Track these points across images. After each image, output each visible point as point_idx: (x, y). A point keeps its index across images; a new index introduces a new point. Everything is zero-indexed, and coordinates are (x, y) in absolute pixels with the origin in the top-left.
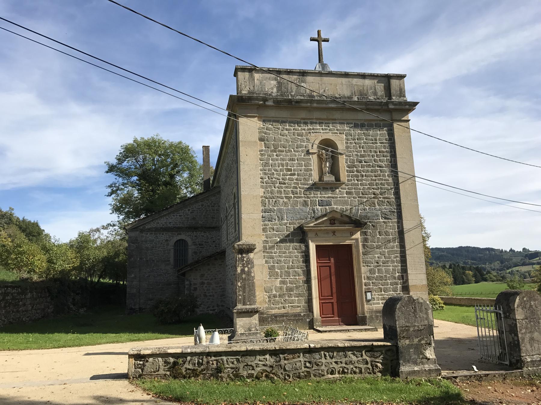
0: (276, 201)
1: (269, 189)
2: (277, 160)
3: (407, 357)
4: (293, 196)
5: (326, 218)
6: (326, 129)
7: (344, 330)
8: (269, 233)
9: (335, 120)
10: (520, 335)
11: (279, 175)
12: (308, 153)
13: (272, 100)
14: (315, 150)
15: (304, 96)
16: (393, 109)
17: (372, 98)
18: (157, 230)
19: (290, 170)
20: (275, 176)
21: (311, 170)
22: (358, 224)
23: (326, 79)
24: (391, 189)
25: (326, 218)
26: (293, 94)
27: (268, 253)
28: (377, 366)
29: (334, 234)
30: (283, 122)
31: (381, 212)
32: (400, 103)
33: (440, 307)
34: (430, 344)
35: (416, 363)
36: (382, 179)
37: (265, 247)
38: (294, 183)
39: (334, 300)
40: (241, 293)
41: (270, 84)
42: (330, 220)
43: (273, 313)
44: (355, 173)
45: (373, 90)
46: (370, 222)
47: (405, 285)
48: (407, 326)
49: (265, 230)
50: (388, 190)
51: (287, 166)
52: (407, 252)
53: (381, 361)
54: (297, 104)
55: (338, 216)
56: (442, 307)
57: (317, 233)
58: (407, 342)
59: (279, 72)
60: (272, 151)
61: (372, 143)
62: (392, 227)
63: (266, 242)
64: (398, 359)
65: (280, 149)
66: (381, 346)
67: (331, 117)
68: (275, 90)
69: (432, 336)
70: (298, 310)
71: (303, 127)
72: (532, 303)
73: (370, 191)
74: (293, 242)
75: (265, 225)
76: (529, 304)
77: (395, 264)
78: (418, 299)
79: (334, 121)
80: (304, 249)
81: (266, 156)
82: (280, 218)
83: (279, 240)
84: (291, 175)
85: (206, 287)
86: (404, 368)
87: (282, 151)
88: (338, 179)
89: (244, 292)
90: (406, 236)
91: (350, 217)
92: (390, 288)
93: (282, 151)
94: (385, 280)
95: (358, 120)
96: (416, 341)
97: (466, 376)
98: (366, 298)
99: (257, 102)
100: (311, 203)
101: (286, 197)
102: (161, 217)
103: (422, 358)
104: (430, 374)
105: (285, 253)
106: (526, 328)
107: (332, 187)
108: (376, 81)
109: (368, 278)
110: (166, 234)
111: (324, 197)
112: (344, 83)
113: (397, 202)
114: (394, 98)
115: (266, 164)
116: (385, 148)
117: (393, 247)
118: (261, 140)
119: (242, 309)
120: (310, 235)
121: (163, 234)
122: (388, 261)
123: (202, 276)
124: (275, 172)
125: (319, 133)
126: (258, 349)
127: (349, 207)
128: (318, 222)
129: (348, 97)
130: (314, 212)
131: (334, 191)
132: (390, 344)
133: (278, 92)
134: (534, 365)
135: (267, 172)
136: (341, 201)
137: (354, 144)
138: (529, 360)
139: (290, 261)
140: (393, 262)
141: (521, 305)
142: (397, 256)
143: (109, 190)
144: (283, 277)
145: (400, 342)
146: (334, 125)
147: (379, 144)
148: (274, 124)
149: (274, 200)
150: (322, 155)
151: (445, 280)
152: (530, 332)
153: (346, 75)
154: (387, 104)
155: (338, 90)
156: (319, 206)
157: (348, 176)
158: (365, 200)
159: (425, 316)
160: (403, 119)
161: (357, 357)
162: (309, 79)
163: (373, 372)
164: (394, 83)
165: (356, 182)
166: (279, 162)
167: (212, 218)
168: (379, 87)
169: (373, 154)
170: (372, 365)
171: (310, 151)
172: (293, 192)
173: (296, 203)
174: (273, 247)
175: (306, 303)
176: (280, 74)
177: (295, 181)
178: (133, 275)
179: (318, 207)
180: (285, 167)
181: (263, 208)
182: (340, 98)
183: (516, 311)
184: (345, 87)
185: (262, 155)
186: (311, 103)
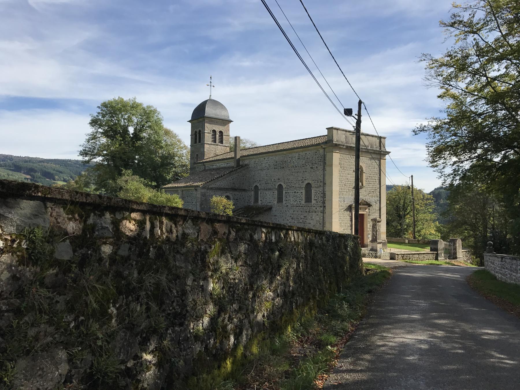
164: (382, 140)
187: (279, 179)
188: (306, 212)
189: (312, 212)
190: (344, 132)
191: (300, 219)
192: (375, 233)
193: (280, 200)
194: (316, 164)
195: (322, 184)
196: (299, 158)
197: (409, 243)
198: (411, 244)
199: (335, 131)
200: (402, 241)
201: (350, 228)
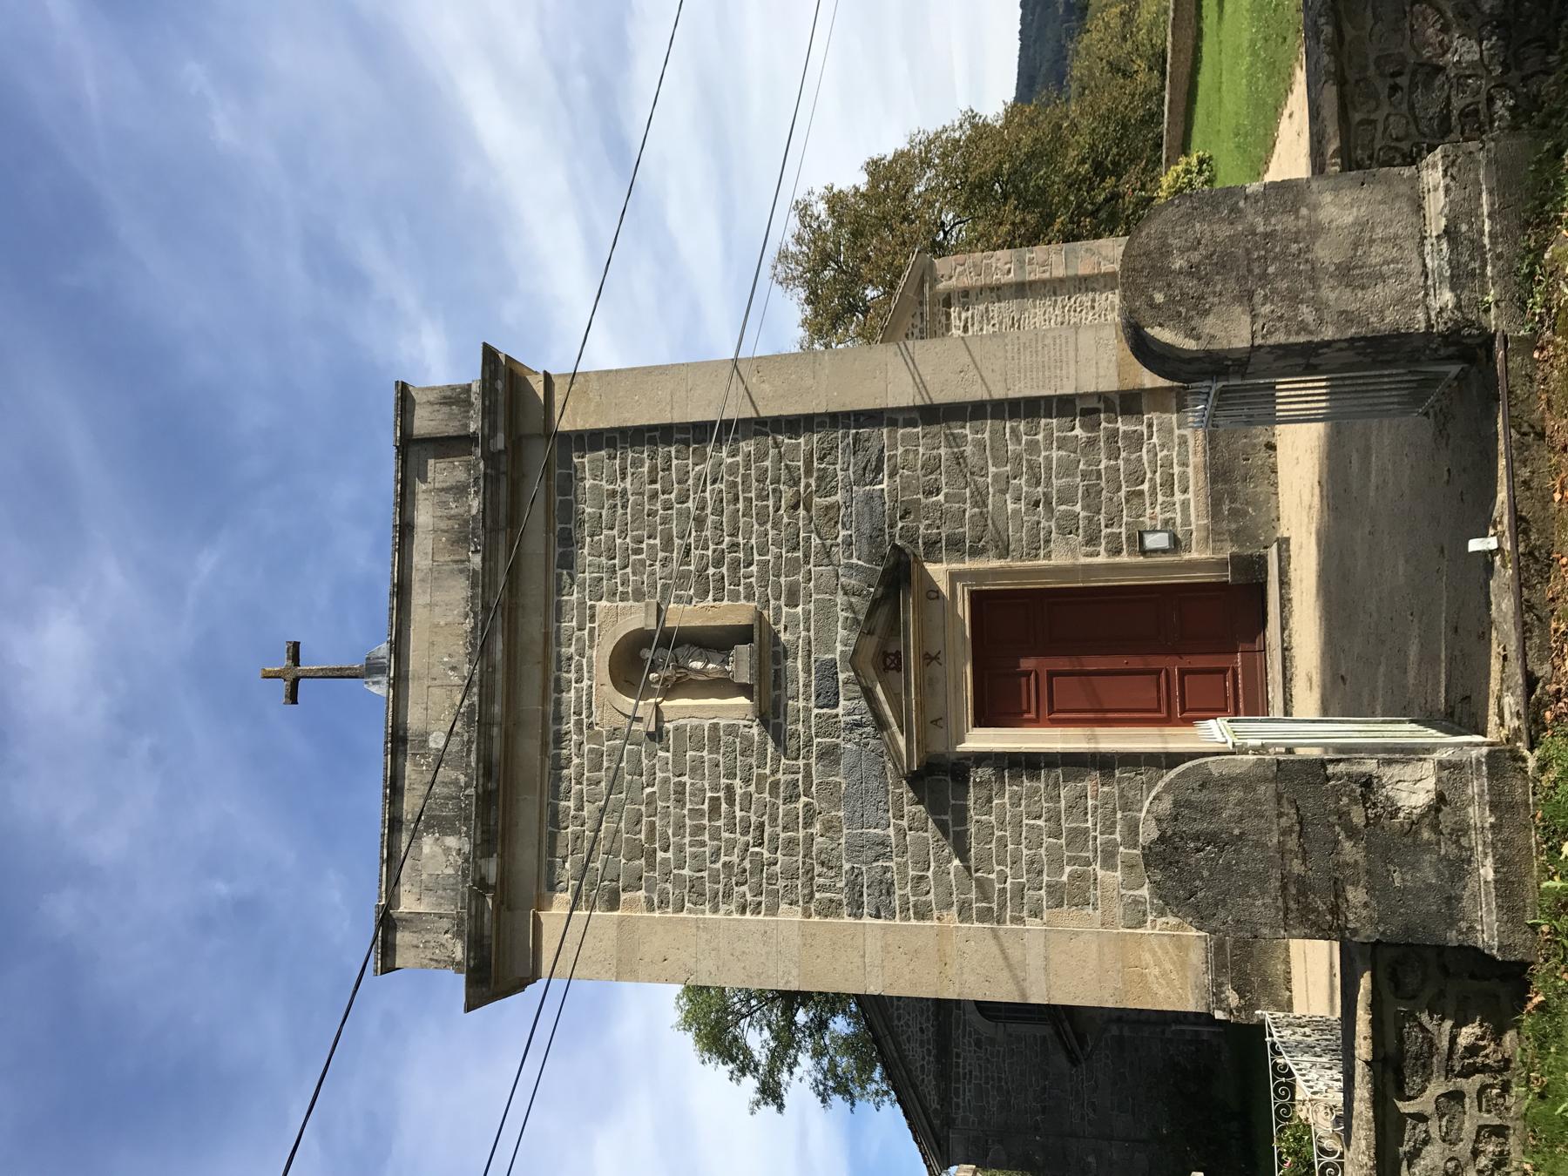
0: (823, 864)
1: (781, 883)
2: (681, 848)
3: (1432, 904)
4: (803, 799)
5: (879, 689)
6: (579, 669)
7: (1284, 668)
8: (931, 896)
9: (546, 636)
10: (1328, 333)
11: (732, 844)
12: (657, 736)
13: (482, 862)
14: (646, 707)
16: (508, 437)
17: (475, 504)
18: (945, 1075)
19: (715, 802)
20: (735, 859)
21: (715, 727)
22: (897, 576)
23: (415, 662)
24: (777, 445)
25: (879, 689)
26: (462, 779)
27: (1002, 906)
28: (1472, 1050)
29: (936, 658)
30: (555, 819)
31: (856, 483)
32: (488, 412)
33: (1200, 172)
34: (1368, 783)
35: (1460, 867)
36: (746, 477)
37: (984, 915)
38: (760, 791)
39: (1174, 665)
42: (887, 668)
44: (724, 570)
45: (450, 498)
46: (892, 526)
47: (1117, 402)
48: (1284, 888)
49: (922, 909)
50: (781, 457)
51: (701, 813)
52: (998, 394)
53: (1448, 1024)
54: (495, 770)
55: (871, 644)
56: (1201, 162)
57: (932, 722)
58: (1356, 895)
59: (394, 824)
60: (651, 866)
61: (624, 507)
62: (910, 448)
63: (964, 912)
64: (1441, 949)
65: (643, 836)
66: (1376, 1024)
67: (539, 650)
68: (451, 841)
69: (1331, 769)
71: (569, 749)
72: (1178, 263)
73: (785, 520)
74: (966, 809)
75: (905, 909)
76: (1181, 281)
77: (1040, 437)
78: (1159, 820)
79: (551, 639)
80: (990, 771)
81: (669, 886)
83: (956, 862)
84: (731, 801)
86: (1487, 929)
87: (652, 825)
88: (743, 634)
90: (940, 398)
91: (875, 605)
92: (1127, 460)
93: (652, 825)
94: (1099, 477)
95: (547, 554)
96: (1350, 851)
97: (1525, 631)
98: (1164, 551)
99: (486, 916)
101: (807, 825)
102: (903, 1058)
103: (1435, 828)
104: (1511, 807)
105: (1002, 842)
106: (1294, 299)
107: (772, 657)
108: (421, 487)
109: (1092, 540)
111: (807, 685)
112: (427, 599)
113: (822, 425)
114: (473, 427)
115: (696, 890)
116: (637, 463)
117: (980, 445)
120: (938, 747)
121: (958, 1056)
122: (1030, 467)
124: (723, 859)
125: (590, 694)
127: (840, 599)
128: (892, 720)
129: (473, 586)
130: (859, 725)
131: (785, 651)
132: (1367, 975)
133: (456, 832)
134: (1472, 274)
135: (721, 887)
136: (820, 626)
137: (629, 570)
138: (1447, 297)
139: (1032, 827)
140: (1033, 447)
141: (1188, 319)
142: (1013, 430)
143: (837, 1099)
144: (1091, 855)
145: (1355, 932)
146: (563, 638)
148: (560, 851)
149: (818, 869)
150: (665, 679)
151: (1116, 23)
152: (1312, 280)
153: (402, 590)
154: (490, 457)
155: (450, 619)
156: (836, 705)
157: (735, 596)
158: (815, 540)
159: (1236, 794)
161: (1426, 1142)
162: (414, 718)
163: (1500, 1071)
164: (425, 422)
165: (754, 568)
166: (687, 840)
168: (440, 477)
169: (659, 506)
170: (1467, 1073)
171: (652, 728)
172: (792, 798)
173: (830, 790)
174: (982, 885)
176: (401, 822)
177: (752, 788)
178: (1091, 1159)
179: (840, 710)
180: (706, 822)
181: (846, 910)
182: (476, 614)
183: (1215, 346)
184: (440, 597)
185: (663, 903)
186: (491, 725)
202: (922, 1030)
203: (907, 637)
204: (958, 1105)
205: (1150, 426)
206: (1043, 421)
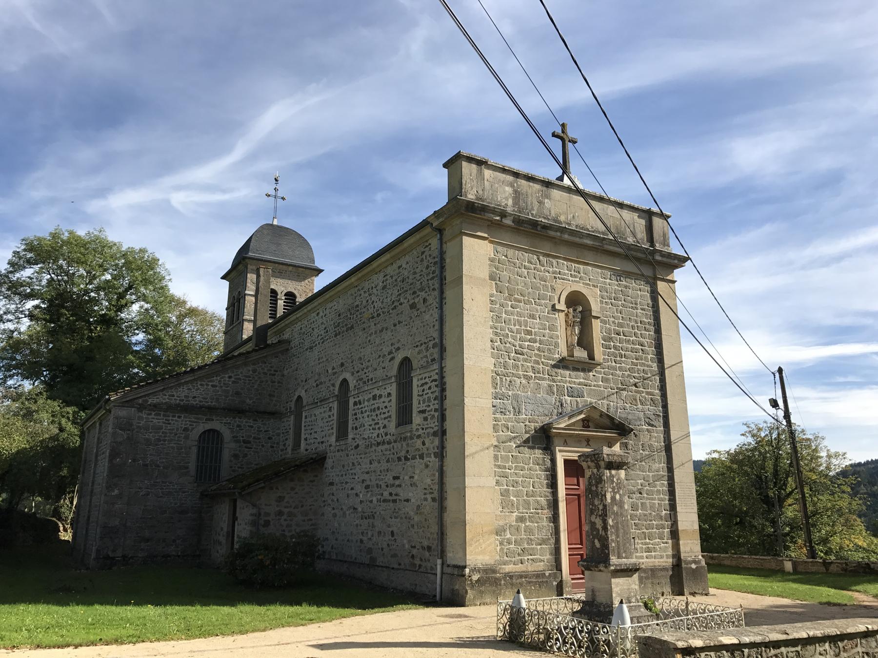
2: (512, 314)
6: (575, 277)
15: (548, 219)
17: (631, 240)
18: (170, 408)
19: (529, 333)
20: (510, 340)
40: (614, 537)
41: (505, 191)
43: (507, 571)
51: (526, 326)
57: (567, 440)
70: (540, 566)
75: (496, 420)
82: (517, 410)
85: (285, 520)
88: (591, 357)
89: (618, 536)
93: (520, 301)
100: (558, 389)
102: (179, 385)
107: (587, 366)
110: (185, 417)
114: (657, 245)
118: (492, 278)
119: (621, 565)
120: (556, 441)
121: (179, 417)
123: (280, 499)
126: (820, 635)
135: (499, 331)
136: (596, 391)
147: (639, 311)
160: (668, 278)
164: (657, 222)
165: (614, 364)
167: (270, 395)
171: (557, 307)
175: (551, 554)
178: (116, 492)
179: (566, 397)
187: (342, 365)
188: (399, 459)
189: (414, 458)
190: (510, 178)
191: (383, 486)
192: (599, 523)
193: (342, 432)
194: (422, 290)
195: (435, 353)
196: (384, 288)
197: (796, 571)
198: (803, 574)
199: (468, 169)
200: (773, 565)
201: (547, 513)
202: (194, 397)
203: (581, 430)
204: (150, 414)
205: (666, 543)
206: (667, 497)
